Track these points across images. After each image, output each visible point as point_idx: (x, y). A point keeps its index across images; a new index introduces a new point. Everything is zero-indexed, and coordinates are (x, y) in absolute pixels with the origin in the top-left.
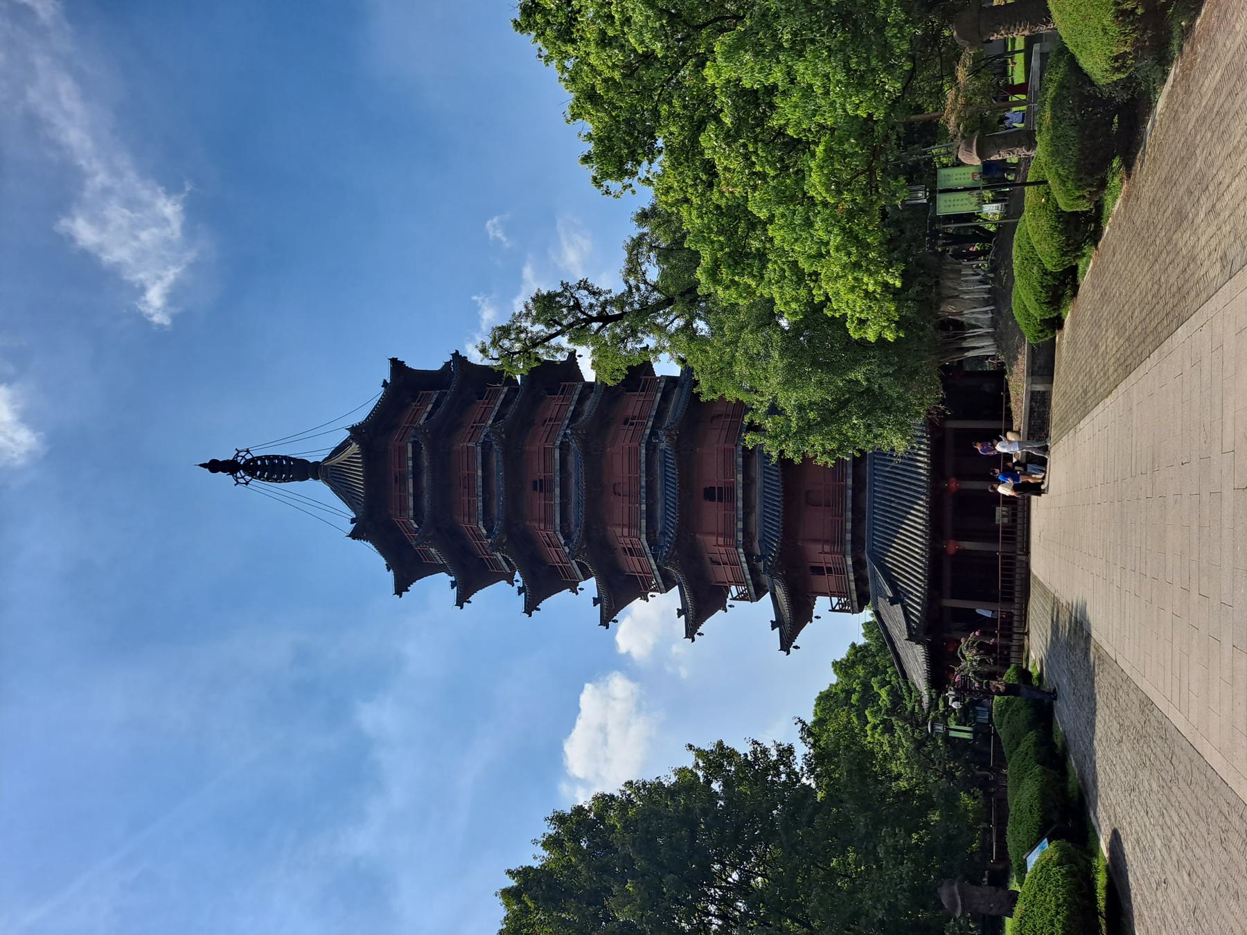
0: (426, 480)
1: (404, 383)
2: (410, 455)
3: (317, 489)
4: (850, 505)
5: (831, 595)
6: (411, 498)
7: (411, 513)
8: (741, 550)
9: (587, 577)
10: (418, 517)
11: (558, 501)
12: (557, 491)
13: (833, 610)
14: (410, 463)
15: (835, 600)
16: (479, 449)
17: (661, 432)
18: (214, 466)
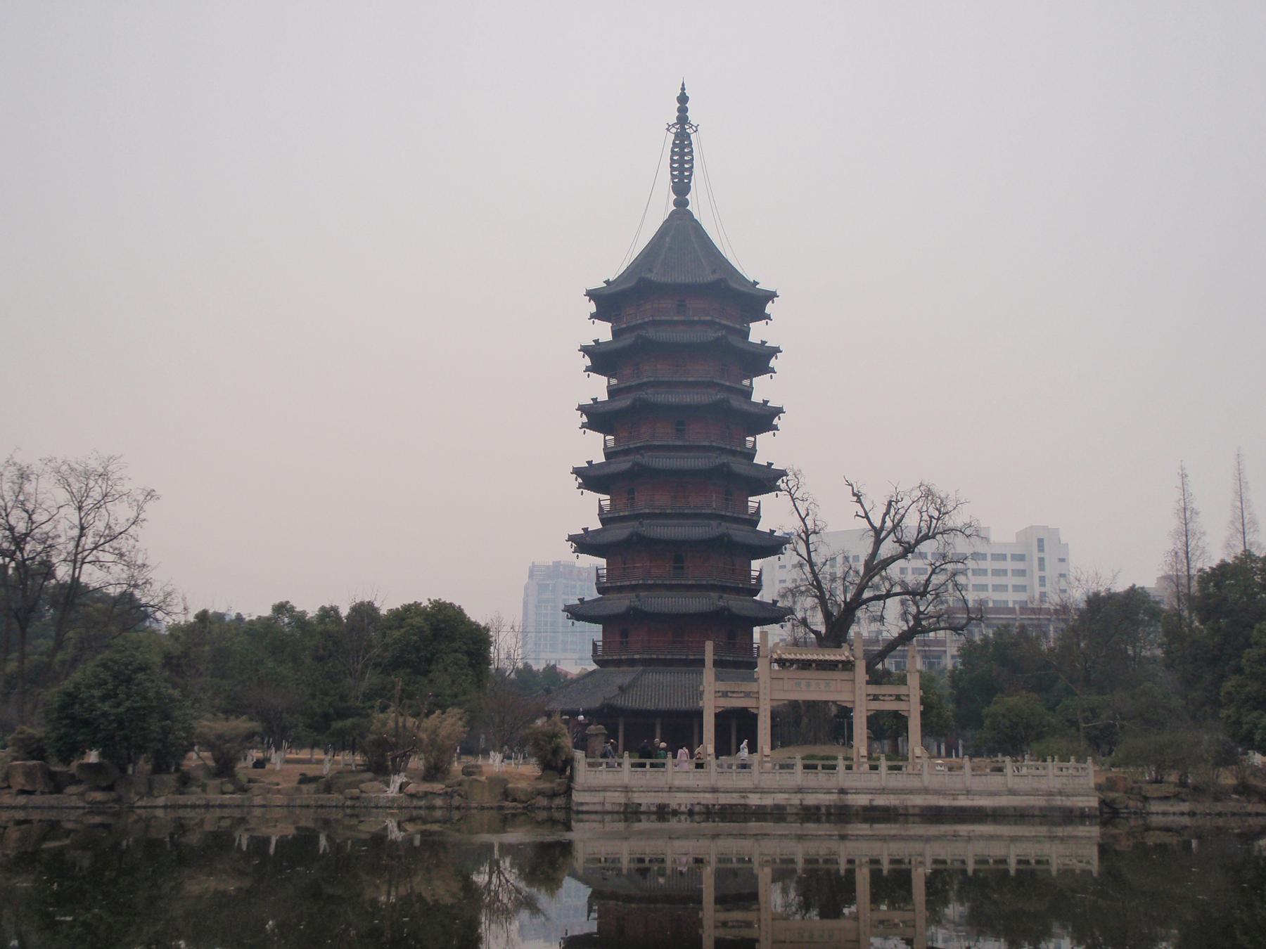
1: (754, 303)
3: (664, 205)
6: (668, 318)
9: (615, 333)
11: (671, 443)
14: (696, 318)
18: (683, 99)
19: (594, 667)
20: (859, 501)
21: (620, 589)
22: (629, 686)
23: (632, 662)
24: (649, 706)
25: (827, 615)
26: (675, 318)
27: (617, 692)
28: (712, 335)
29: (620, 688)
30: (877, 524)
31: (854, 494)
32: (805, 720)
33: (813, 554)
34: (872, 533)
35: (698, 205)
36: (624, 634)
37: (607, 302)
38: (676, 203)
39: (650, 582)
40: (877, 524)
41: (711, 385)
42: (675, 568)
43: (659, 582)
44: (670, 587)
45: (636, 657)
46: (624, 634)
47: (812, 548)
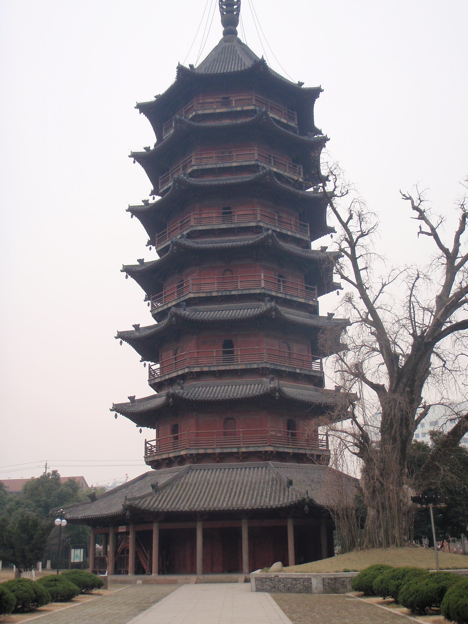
0: (226, 122)
1: (302, 100)
2: (246, 108)
4: (225, 451)
5: (158, 440)
6: (212, 111)
7: (200, 112)
8: (186, 370)
10: (197, 118)
11: (216, 227)
12: (224, 226)
13: (146, 443)
14: (239, 109)
15: (154, 443)
16: (253, 163)
17: (273, 304)
19: (149, 469)
20: (422, 216)
21: (169, 462)
22: (166, 485)
23: (181, 460)
24: (183, 506)
25: (391, 359)
26: (218, 111)
27: (150, 490)
28: (264, 307)
29: (154, 486)
30: (450, 247)
31: (415, 208)
32: (371, 513)
33: (363, 274)
34: (444, 260)
35: (246, 32)
36: (175, 429)
37: (157, 111)
38: (225, 33)
39: (196, 370)
40: (450, 247)
41: (259, 297)
42: (225, 352)
43: (206, 369)
44: (221, 374)
45: (183, 453)
46: (175, 429)
47: (361, 264)
